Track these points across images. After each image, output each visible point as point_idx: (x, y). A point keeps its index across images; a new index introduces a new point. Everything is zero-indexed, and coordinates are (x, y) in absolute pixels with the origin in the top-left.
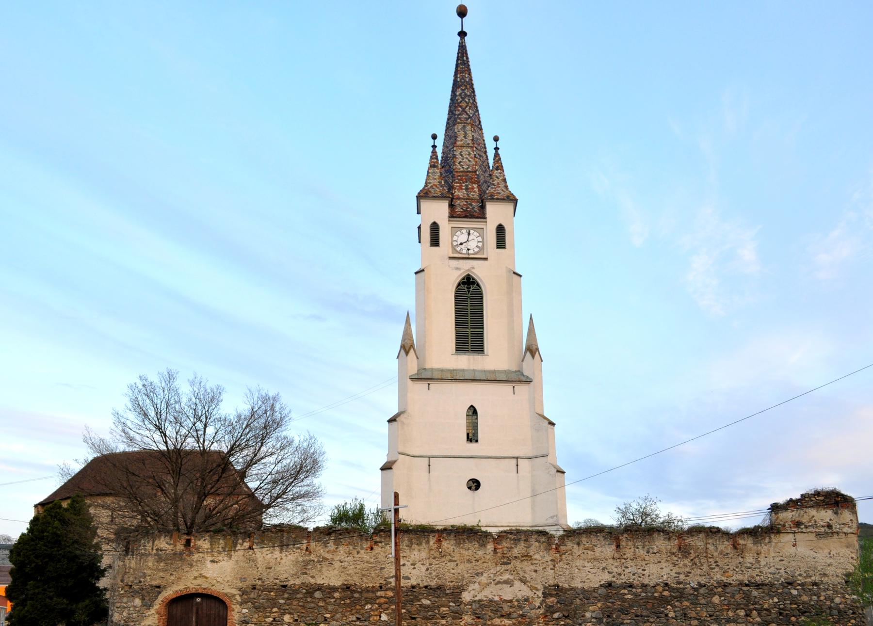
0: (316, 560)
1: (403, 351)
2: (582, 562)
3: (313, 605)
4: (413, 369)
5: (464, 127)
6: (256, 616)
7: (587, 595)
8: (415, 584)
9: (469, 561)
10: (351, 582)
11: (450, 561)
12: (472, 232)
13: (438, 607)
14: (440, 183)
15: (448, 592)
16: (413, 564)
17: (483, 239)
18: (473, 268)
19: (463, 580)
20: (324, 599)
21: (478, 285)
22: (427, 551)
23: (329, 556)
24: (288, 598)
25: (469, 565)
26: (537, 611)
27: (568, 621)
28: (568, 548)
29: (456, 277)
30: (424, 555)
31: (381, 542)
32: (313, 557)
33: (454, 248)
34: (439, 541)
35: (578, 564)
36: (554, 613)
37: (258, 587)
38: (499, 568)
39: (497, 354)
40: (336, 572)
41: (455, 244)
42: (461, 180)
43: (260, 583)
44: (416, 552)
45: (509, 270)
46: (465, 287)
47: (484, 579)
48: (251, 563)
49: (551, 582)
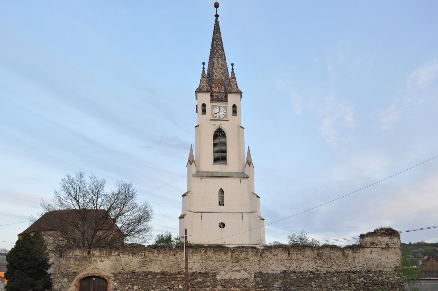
2: (272, 261)
3: (147, 281)
5: (218, 59)
7: (275, 276)
8: (195, 271)
9: (220, 261)
10: (165, 271)
11: (211, 261)
13: (206, 282)
15: (210, 275)
16: (194, 262)
17: (226, 111)
18: (222, 125)
20: (152, 279)
21: (224, 132)
23: (155, 259)
24: (136, 278)
25: (220, 263)
27: (266, 289)
28: (266, 255)
29: (213, 129)
30: (199, 258)
31: (179, 252)
32: (147, 259)
33: (213, 116)
34: (206, 251)
37: (122, 273)
38: (234, 264)
39: (233, 164)
40: (158, 266)
41: (213, 113)
43: (122, 271)
44: (195, 257)
46: (218, 134)
47: (227, 269)
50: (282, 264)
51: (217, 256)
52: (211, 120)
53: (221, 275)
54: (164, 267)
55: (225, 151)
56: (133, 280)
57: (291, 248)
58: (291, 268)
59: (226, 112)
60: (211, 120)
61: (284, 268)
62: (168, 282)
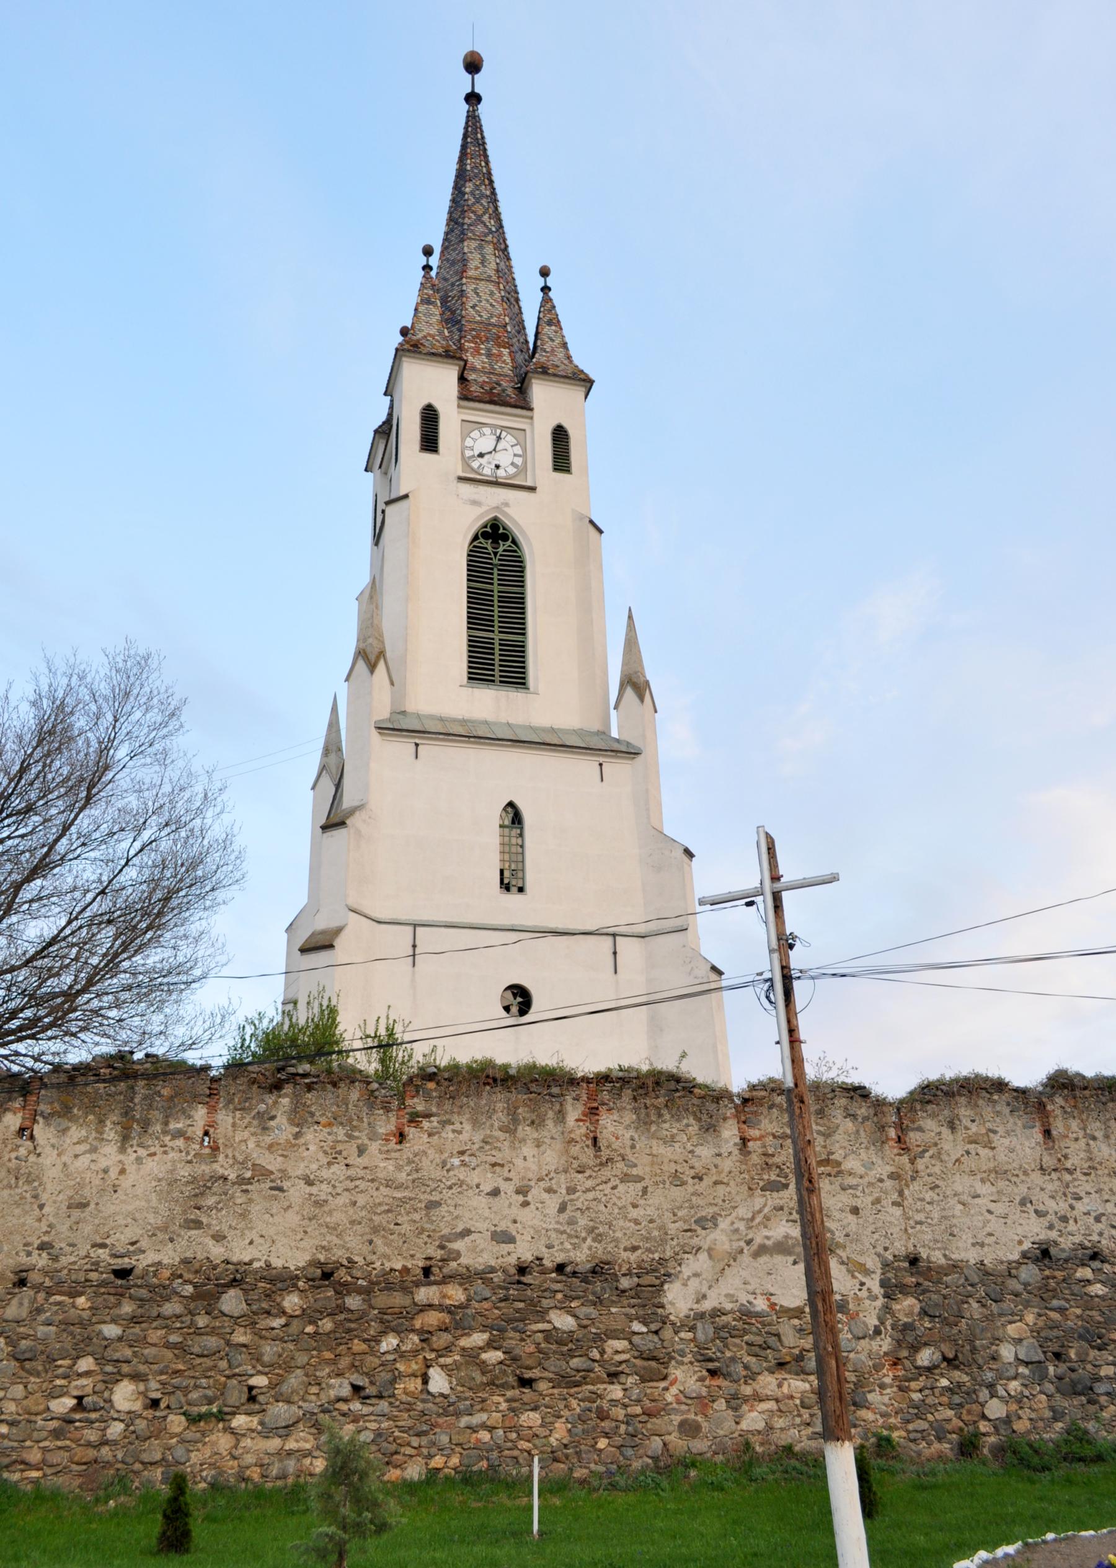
0: (232, 1177)
1: (361, 665)
2: (967, 1180)
3: (212, 1342)
4: (382, 711)
5: (481, 247)
6: (18, 1391)
7: (993, 1282)
8: (528, 1257)
9: (677, 1180)
10: (339, 1255)
11: (626, 1178)
12: (504, 434)
13: (599, 1339)
14: (441, 333)
15: (625, 1283)
16: (522, 1191)
17: (524, 450)
18: (507, 505)
19: (663, 1242)
20: (249, 1320)
21: (514, 542)
22: (558, 1145)
23: (272, 1162)
24: (134, 1320)
25: (677, 1193)
26: (875, 1345)
27: (957, 1375)
28: (929, 1137)
29: (471, 521)
30: (552, 1158)
31: (428, 1116)
32: (222, 1166)
33: (466, 461)
34: (593, 1112)
35: (959, 1188)
36: (915, 1349)
37: (34, 1277)
38: (758, 1202)
39: (555, 691)
40: (292, 1218)
41: (468, 453)
42: (478, 336)
43: (41, 1260)
44: (528, 1150)
45: (581, 517)
46: (488, 544)
47: (720, 1238)
48: (23, 1188)
49: (900, 1247)
50: (1023, 1203)
51: (659, 1149)
52: (461, 479)
53: (694, 1283)
54: (332, 1229)
55: (520, 628)
56: (111, 1331)
57: (1051, 1097)
58: (1071, 1226)
59: (524, 455)
60: (461, 479)
61: (1034, 1230)
62: (358, 1346)
